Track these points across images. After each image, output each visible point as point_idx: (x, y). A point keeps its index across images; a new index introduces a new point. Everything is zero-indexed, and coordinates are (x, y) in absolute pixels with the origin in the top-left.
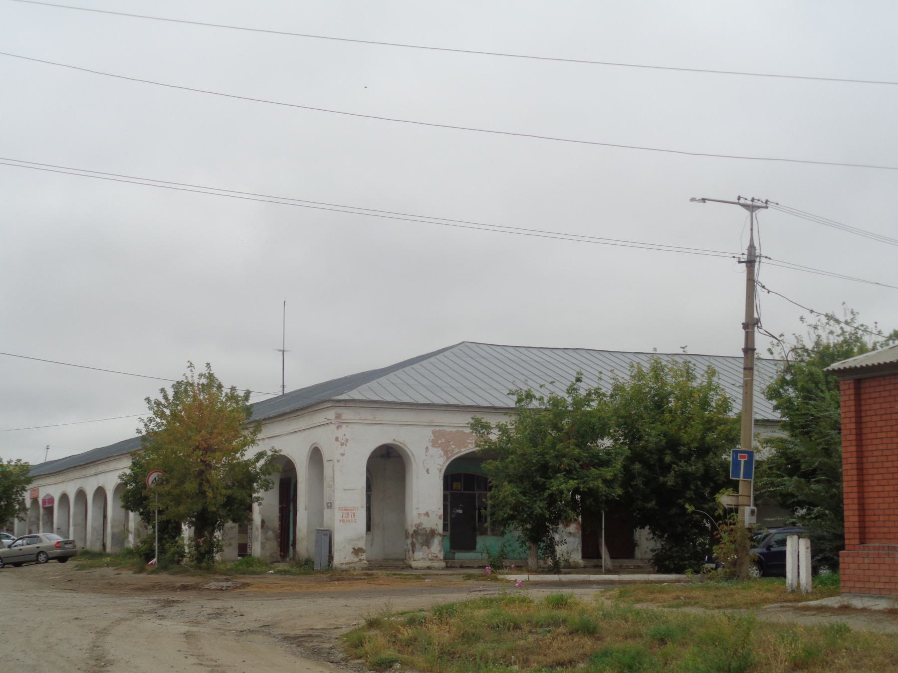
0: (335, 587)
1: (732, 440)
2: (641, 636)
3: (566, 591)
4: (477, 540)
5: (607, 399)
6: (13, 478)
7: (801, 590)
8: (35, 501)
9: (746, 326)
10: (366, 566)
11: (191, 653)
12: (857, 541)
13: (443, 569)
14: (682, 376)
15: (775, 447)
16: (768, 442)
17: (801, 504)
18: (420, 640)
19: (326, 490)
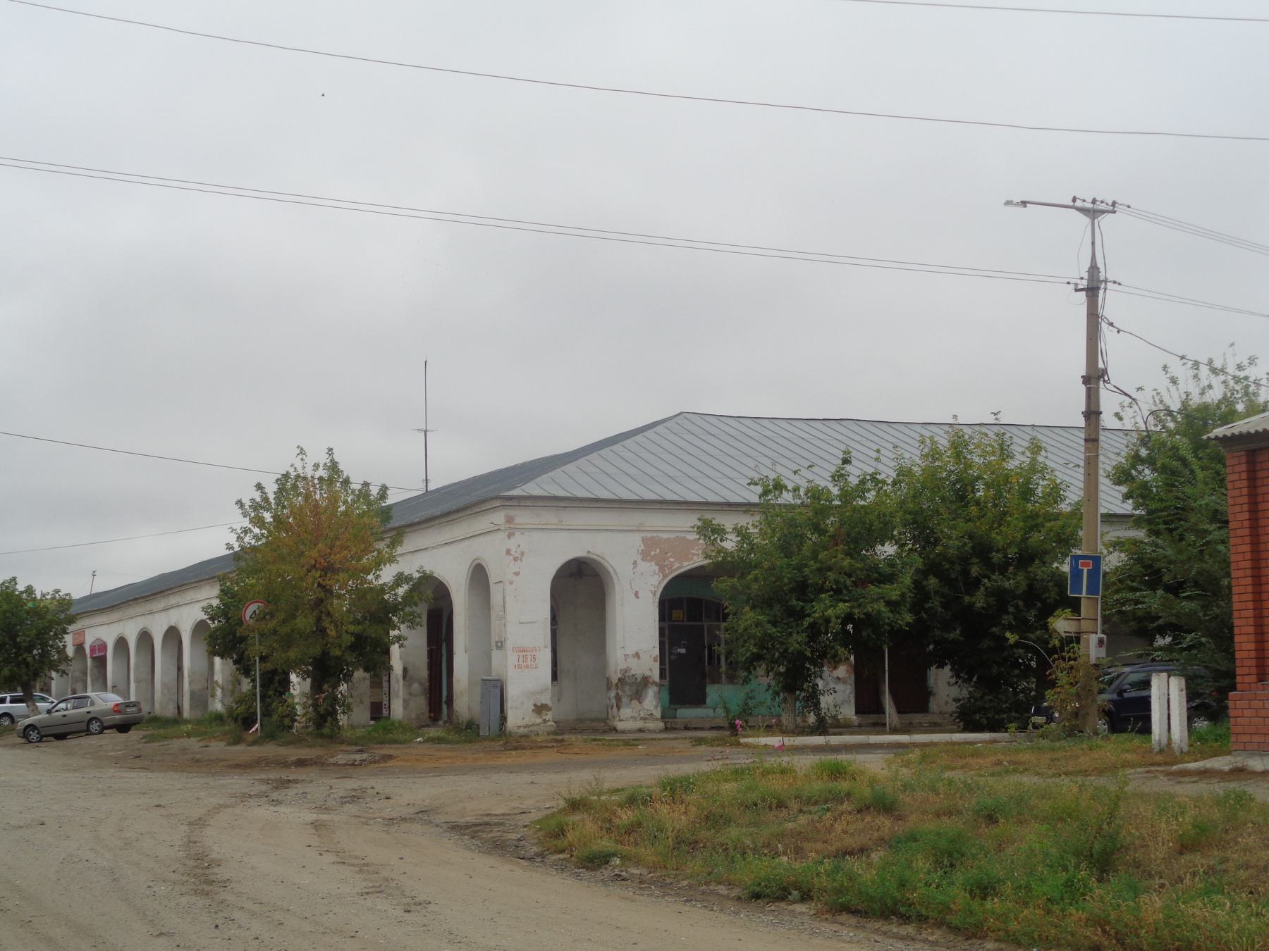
0: (513, 758)
1: (1066, 541)
2: (959, 812)
3: (842, 757)
4: (707, 691)
5: (888, 488)
6: (49, 617)
7: (1173, 749)
8: (80, 648)
9: (1087, 380)
10: (553, 729)
11: (325, 849)
12: (1253, 678)
13: (661, 731)
14: (993, 453)
15: (1127, 550)
16: (1117, 545)
17: (1162, 631)
18: (645, 825)
19: (495, 624)
